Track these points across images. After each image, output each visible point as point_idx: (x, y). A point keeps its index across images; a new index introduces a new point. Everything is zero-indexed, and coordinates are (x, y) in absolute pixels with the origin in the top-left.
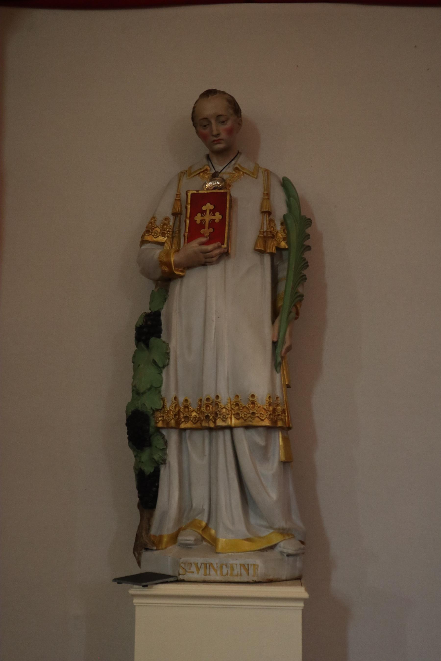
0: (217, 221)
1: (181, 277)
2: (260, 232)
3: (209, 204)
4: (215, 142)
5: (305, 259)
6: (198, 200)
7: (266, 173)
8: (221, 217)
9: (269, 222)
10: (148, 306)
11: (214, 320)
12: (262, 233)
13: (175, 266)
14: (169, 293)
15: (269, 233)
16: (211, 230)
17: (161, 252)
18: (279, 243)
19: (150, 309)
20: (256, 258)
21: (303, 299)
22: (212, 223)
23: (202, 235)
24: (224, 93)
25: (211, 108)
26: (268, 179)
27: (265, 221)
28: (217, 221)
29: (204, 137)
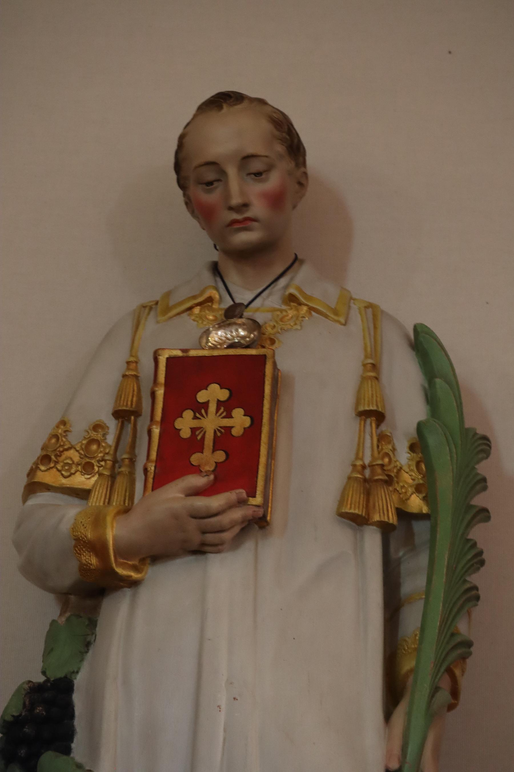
0: (237, 432)
1: (134, 584)
2: (354, 466)
3: (214, 387)
4: (236, 226)
5: (474, 545)
6: (185, 375)
7: (370, 311)
8: (247, 421)
9: (378, 441)
10: (39, 665)
11: (223, 707)
12: (359, 468)
13: (118, 553)
14: (97, 629)
15: (379, 470)
16: (221, 456)
17: (80, 513)
18: (405, 501)
19: (44, 673)
20: (342, 536)
21: (470, 654)
22: (223, 438)
23: (197, 470)
24: (262, 102)
25: (228, 137)
26: (375, 328)
27: (368, 437)
28: (237, 432)
29: (203, 213)
